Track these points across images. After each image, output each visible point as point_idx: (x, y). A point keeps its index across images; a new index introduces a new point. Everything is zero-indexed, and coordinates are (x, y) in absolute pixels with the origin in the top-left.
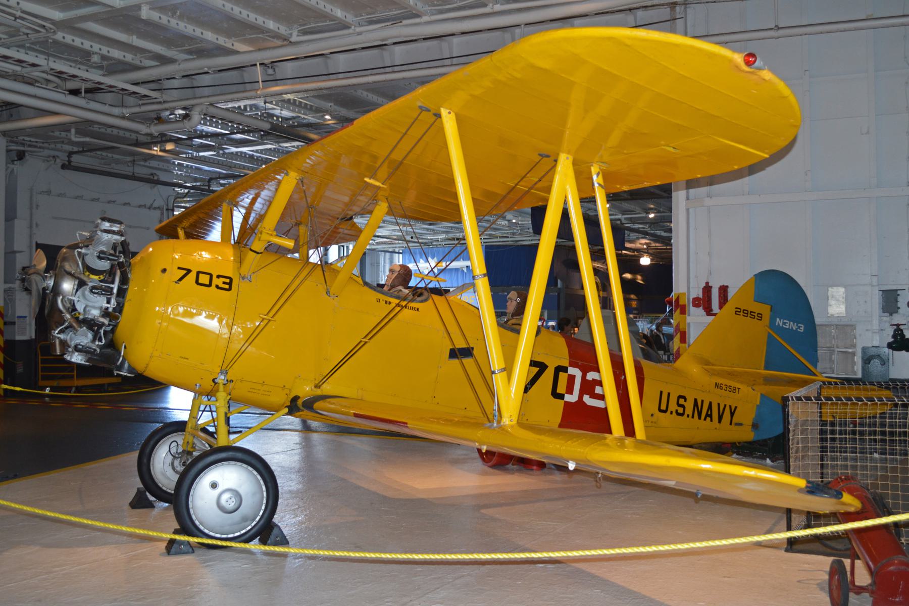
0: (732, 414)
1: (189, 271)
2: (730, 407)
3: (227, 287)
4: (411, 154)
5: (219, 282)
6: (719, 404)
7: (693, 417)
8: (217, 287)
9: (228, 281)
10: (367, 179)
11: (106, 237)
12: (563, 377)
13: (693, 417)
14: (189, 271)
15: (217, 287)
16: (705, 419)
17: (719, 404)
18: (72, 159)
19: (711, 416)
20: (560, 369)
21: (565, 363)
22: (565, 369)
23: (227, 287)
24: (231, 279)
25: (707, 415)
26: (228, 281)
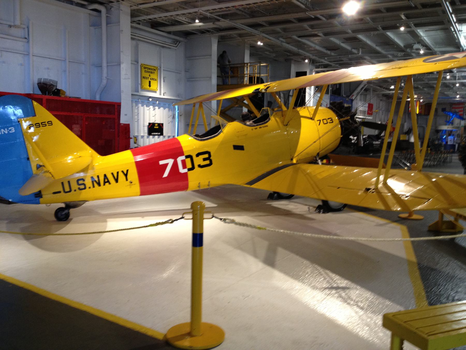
0: (126, 175)
1: (320, 121)
2: (123, 172)
3: (207, 162)
4: (440, 317)
5: (329, 121)
6: (112, 174)
7: (94, 187)
8: (200, 166)
9: (206, 156)
10: (166, 175)
11: (360, 53)
12: (189, 165)
13: (94, 187)
14: (320, 121)
15: (200, 166)
16: (104, 185)
17: (112, 174)
18: (185, 227)
19: (108, 182)
20: (193, 168)
21: (190, 173)
22: (189, 170)
23: (207, 162)
24: (208, 153)
25: (105, 183)
26: (206, 156)
